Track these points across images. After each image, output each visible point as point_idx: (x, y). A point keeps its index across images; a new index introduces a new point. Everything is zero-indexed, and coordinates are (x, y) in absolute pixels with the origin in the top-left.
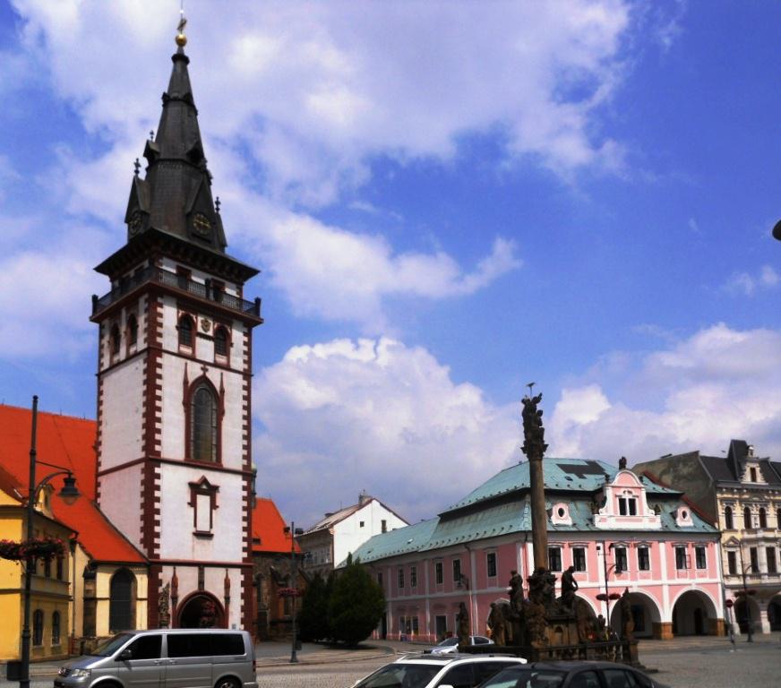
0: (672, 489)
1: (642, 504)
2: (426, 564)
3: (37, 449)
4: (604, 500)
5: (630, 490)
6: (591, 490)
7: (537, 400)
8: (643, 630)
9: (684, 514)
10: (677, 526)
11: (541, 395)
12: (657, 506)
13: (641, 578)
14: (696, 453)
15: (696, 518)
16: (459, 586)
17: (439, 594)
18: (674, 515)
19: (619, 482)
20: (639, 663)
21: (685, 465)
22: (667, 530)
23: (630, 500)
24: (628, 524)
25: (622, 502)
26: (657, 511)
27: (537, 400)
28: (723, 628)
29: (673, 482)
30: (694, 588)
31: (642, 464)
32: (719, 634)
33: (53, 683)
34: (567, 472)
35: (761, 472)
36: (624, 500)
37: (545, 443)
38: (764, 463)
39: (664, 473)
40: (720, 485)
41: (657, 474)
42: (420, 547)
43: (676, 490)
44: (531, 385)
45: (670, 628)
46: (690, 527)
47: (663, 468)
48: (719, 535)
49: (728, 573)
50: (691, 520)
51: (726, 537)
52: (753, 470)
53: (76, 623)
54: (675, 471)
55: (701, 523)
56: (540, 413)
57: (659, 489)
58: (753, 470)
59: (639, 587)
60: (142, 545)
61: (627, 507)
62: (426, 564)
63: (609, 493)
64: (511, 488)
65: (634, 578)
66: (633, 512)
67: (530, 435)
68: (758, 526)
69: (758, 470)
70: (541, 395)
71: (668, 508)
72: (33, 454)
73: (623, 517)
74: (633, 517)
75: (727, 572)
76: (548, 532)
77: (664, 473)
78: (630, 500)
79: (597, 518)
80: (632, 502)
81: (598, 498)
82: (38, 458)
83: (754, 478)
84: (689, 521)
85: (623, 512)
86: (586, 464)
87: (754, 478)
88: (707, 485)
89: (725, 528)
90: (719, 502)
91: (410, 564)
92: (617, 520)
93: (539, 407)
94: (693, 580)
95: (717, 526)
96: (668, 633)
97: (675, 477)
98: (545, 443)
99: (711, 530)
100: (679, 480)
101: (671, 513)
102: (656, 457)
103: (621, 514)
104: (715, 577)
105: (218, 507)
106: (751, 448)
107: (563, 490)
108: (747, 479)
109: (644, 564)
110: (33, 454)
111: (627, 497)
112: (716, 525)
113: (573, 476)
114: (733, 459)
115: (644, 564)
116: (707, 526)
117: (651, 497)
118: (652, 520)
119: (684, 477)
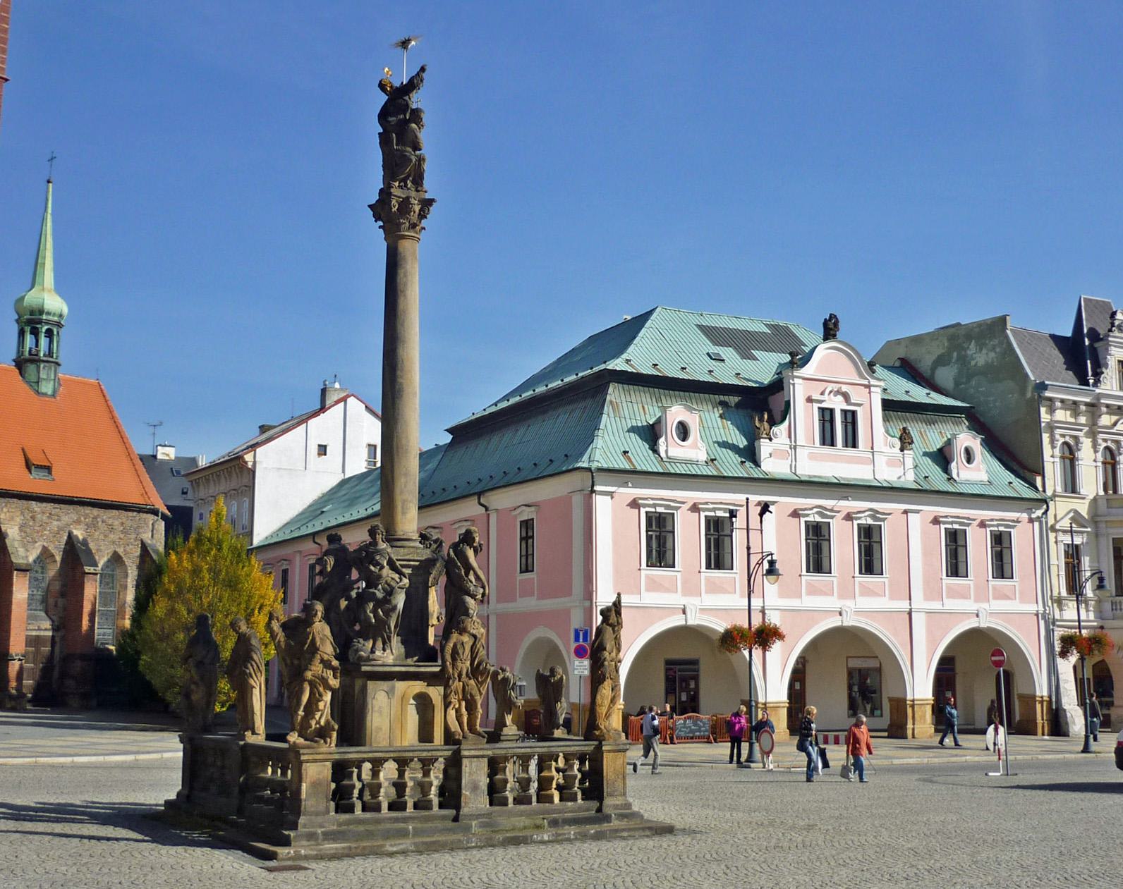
1: (872, 420)
3: (751, 545)
8: (432, 809)
9: (969, 456)
12: (904, 429)
13: (810, 593)
18: (943, 458)
21: (981, 347)
22: (926, 487)
23: (845, 412)
25: (827, 416)
29: (957, 383)
31: (898, 342)
33: (830, 765)
34: (716, 343)
36: (832, 411)
45: (929, 710)
46: (981, 483)
47: (941, 351)
50: (983, 467)
53: (39, 830)
57: (919, 394)
59: (857, 612)
60: (281, 629)
63: (799, 390)
65: (691, 589)
66: (852, 441)
72: (748, 548)
73: (827, 450)
74: (850, 452)
77: (941, 361)
80: (850, 419)
81: (775, 402)
82: (752, 551)
84: (695, 446)
86: (767, 330)
89: (1059, 489)
96: (923, 725)
99: (1027, 492)
103: (823, 443)
109: (870, 563)
110: (748, 548)
111: (838, 404)
113: (728, 353)
115: (870, 563)
116: (1017, 483)
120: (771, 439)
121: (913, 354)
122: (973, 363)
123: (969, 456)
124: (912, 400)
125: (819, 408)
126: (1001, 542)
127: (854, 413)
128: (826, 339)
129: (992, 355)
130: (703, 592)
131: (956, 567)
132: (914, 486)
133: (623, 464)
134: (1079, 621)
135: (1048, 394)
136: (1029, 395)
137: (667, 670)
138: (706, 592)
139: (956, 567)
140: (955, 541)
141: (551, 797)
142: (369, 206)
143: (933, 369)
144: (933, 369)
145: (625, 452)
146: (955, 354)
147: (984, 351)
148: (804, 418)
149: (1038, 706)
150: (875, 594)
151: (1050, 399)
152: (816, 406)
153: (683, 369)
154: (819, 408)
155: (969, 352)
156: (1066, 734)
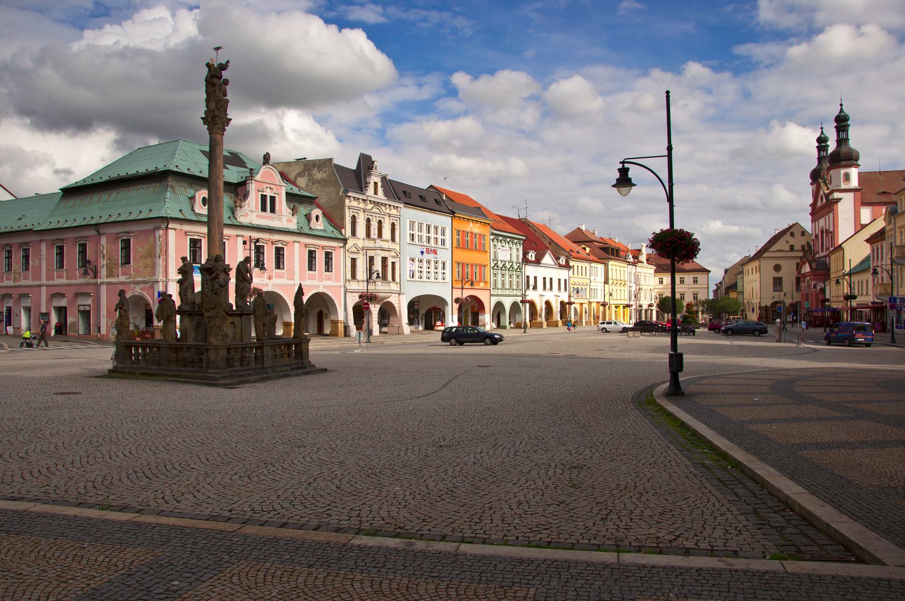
0: (307, 192)
1: (282, 204)
2: (43, 246)
4: (246, 196)
5: (272, 187)
6: (235, 182)
7: (223, 67)
9: (317, 218)
10: (310, 228)
11: (228, 62)
13: (326, 280)
14: (331, 160)
15: (326, 223)
16: (86, 273)
17: (57, 281)
18: (308, 217)
19: (262, 177)
20: (310, 362)
21: (319, 170)
23: (271, 197)
24: (266, 220)
25: (264, 198)
26: (294, 211)
27: (223, 67)
28: (343, 329)
29: (307, 186)
30: (321, 290)
32: (340, 335)
35: (382, 187)
36: (266, 196)
37: (229, 117)
38: (384, 178)
39: (299, 175)
40: (349, 194)
41: (292, 176)
42: (36, 224)
43: (310, 193)
44: (217, 49)
47: (300, 170)
48: (345, 241)
49: (350, 279)
50: (322, 224)
51: (351, 242)
52: (376, 184)
54: (310, 175)
55: (331, 229)
56: (226, 82)
57: (296, 190)
58: (376, 184)
61: (268, 204)
62: (43, 246)
63: (252, 187)
64: (151, 168)
65: (321, 280)
66: (273, 210)
67: (213, 105)
68: (376, 237)
69: (380, 184)
70: (228, 62)
71: (303, 210)
73: (264, 214)
74: (272, 215)
75: (349, 276)
76: (225, 224)
77: (299, 175)
78: (271, 197)
79: (239, 213)
80: (273, 199)
83: (376, 193)
84: (320, 225)
85: (264, 209)
87: (376, 193)
88: (338, 192)
90: (347, 208)
91: (20, 245)
92: (258, 216)
93: (225, 74)
94: (315, 284)
95: (343, 232)
97: (309, 180)
98: (229, 117)
99: (339, 236)
100: (313, 184)
101: (305, 215)
102: (292, 159)
104: (340, 281)
105: (340, 31)
106: (375, 163)
107: (195, 176)
108: (370, 190)
111: (268, 193)
112: (343, 231)
114: (360, 170)
117: (290, 196)
118: (289, 221)
119: (318, 182)
120: (241, 208)
121: (286, 170)
122: (315, 178)
123: (317, 218)
124: (179, 171)
125: (261, 195)
126: (328, 256)
127: (274, 197)
128: (264, 164)
129: (325, 175)
130: (120, 275)
131: (311, 266)
132: (297, 231)
133: (180, 216)
134: (367, 290)
135: (349, 194)
136: (341, 194)
137: (782, 288)
138: (122, 275)
139: (311, 266)
140: (312, 255)
141: (541, 323)
142: (231, 119)
143: (296, 178)
144: (296, 178)
145: (181, 210)
146: (307, 173)
147: (321, 173)
148: (253, 200)
149: (340, 324)
150: (329, 279)
151: (350, 197)
152: (260, 193)
153: (201, 172)
154: (261, 195)
155: (314, 173)
156: (349, 336)
